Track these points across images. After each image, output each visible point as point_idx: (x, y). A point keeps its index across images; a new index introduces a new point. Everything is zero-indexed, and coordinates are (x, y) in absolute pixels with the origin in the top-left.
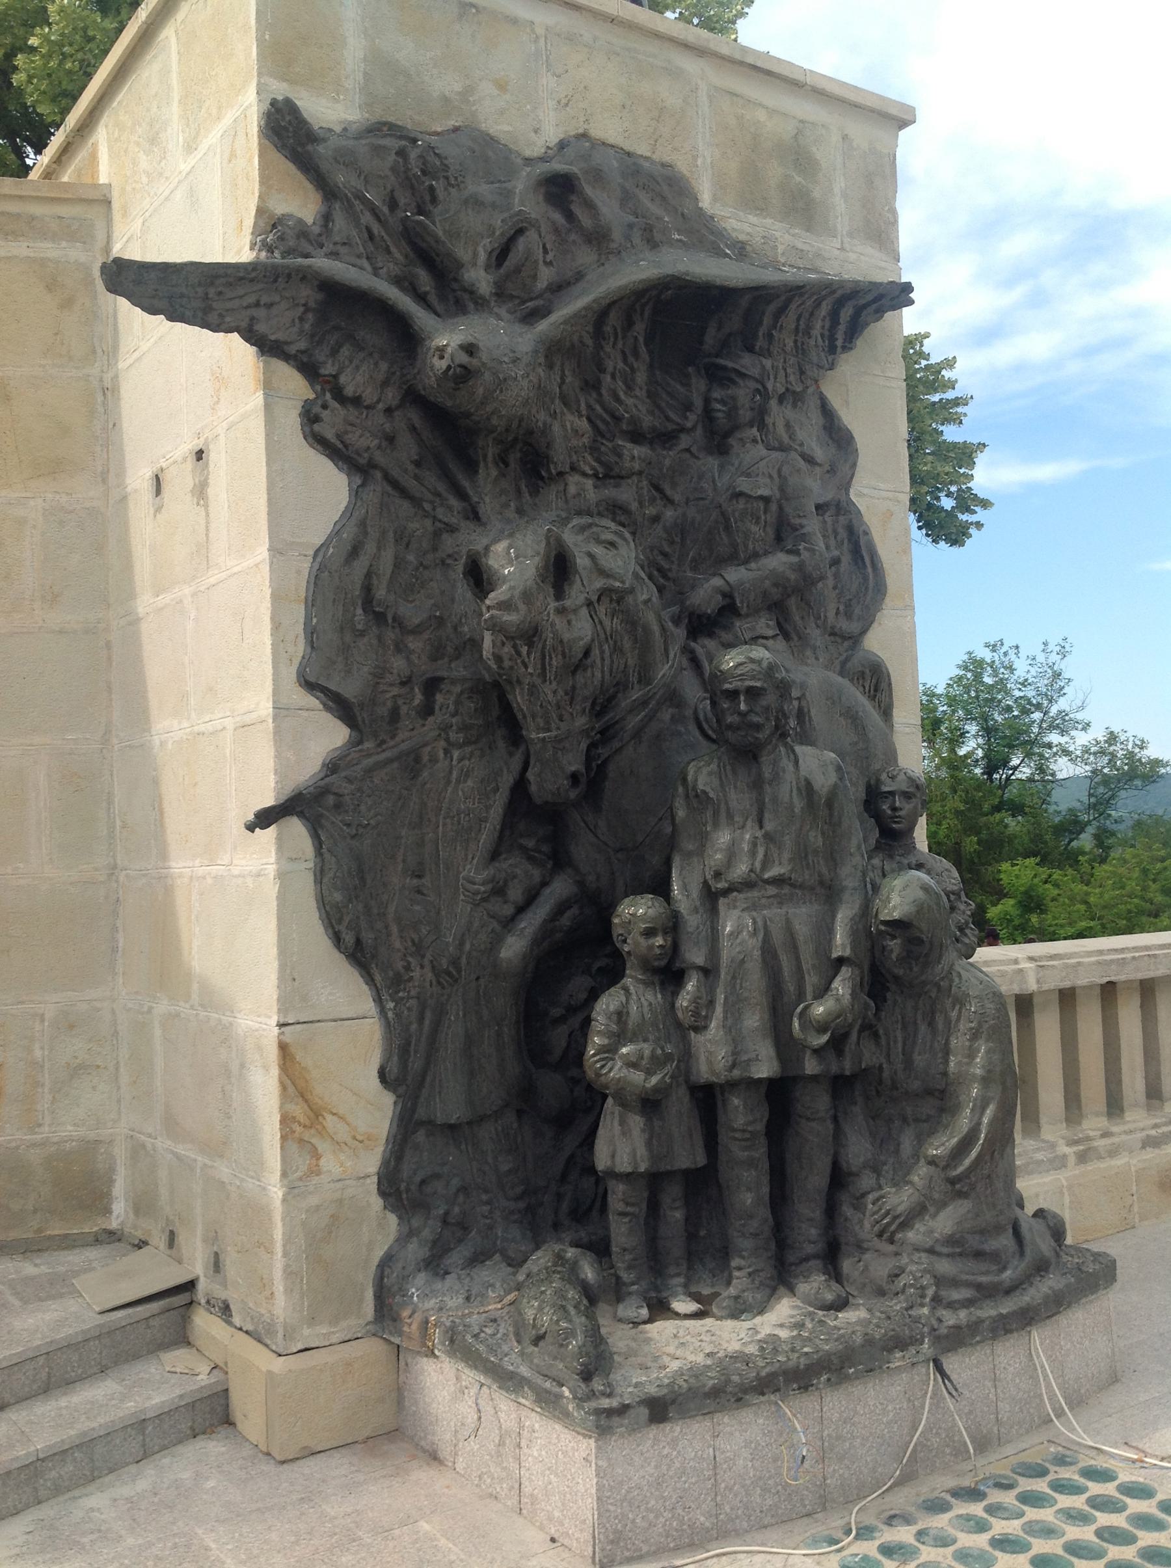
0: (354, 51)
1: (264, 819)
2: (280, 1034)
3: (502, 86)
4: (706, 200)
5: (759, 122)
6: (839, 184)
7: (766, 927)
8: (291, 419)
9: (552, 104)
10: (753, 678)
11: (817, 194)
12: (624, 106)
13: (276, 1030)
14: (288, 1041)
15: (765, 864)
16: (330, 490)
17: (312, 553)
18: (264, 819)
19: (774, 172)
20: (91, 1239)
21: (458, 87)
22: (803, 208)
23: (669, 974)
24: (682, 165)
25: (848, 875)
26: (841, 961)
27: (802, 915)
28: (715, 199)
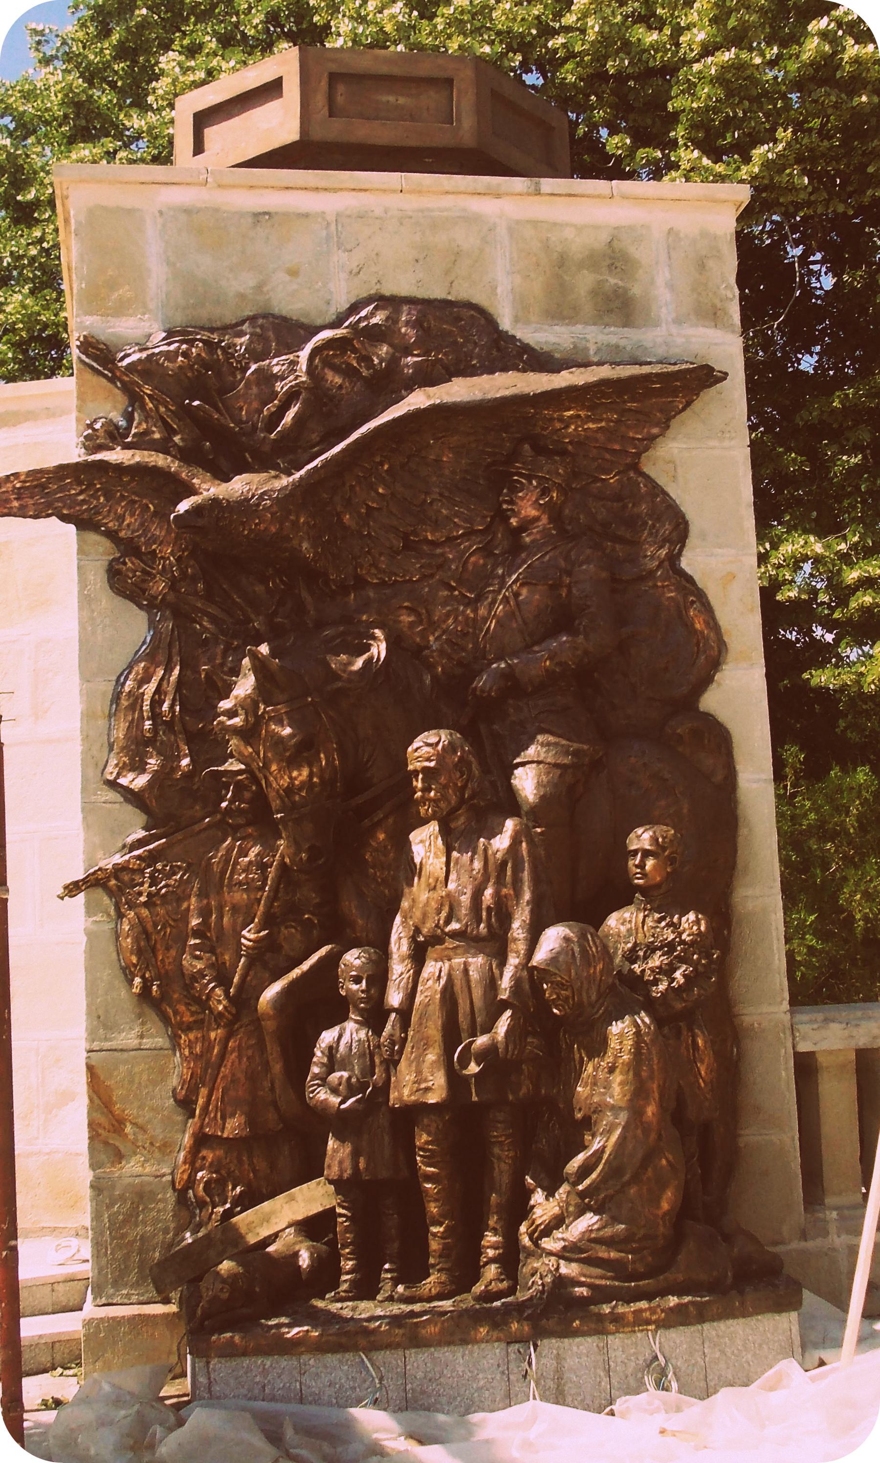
0: (157, 277)
1: (72, 889)
2: (88, 1058)
3: (293, 273)
4: (506, 324)
5: (566, 239)
6: (662, 276)
7: (449, 976)
8: (98, 578)
9: (343, 276)
10: (428, 760)
11: (636, 290)
12: (417, 261)
13: (85, 1055)
14: (93, 1063)
15: (448, 921)
16: (133, 628)
17: (115, 678)
18: (72, 889)
19: (584, 282)
20: (73, 1232)
21: (252, 283)
22: (620, 307)
23: (375, 1016)
24: (479, 298)
25: (518, 929)
26: (504, 1005)
27: (477, 962)
28: (516, 320)
